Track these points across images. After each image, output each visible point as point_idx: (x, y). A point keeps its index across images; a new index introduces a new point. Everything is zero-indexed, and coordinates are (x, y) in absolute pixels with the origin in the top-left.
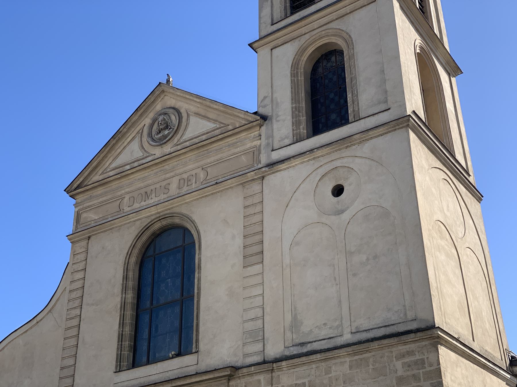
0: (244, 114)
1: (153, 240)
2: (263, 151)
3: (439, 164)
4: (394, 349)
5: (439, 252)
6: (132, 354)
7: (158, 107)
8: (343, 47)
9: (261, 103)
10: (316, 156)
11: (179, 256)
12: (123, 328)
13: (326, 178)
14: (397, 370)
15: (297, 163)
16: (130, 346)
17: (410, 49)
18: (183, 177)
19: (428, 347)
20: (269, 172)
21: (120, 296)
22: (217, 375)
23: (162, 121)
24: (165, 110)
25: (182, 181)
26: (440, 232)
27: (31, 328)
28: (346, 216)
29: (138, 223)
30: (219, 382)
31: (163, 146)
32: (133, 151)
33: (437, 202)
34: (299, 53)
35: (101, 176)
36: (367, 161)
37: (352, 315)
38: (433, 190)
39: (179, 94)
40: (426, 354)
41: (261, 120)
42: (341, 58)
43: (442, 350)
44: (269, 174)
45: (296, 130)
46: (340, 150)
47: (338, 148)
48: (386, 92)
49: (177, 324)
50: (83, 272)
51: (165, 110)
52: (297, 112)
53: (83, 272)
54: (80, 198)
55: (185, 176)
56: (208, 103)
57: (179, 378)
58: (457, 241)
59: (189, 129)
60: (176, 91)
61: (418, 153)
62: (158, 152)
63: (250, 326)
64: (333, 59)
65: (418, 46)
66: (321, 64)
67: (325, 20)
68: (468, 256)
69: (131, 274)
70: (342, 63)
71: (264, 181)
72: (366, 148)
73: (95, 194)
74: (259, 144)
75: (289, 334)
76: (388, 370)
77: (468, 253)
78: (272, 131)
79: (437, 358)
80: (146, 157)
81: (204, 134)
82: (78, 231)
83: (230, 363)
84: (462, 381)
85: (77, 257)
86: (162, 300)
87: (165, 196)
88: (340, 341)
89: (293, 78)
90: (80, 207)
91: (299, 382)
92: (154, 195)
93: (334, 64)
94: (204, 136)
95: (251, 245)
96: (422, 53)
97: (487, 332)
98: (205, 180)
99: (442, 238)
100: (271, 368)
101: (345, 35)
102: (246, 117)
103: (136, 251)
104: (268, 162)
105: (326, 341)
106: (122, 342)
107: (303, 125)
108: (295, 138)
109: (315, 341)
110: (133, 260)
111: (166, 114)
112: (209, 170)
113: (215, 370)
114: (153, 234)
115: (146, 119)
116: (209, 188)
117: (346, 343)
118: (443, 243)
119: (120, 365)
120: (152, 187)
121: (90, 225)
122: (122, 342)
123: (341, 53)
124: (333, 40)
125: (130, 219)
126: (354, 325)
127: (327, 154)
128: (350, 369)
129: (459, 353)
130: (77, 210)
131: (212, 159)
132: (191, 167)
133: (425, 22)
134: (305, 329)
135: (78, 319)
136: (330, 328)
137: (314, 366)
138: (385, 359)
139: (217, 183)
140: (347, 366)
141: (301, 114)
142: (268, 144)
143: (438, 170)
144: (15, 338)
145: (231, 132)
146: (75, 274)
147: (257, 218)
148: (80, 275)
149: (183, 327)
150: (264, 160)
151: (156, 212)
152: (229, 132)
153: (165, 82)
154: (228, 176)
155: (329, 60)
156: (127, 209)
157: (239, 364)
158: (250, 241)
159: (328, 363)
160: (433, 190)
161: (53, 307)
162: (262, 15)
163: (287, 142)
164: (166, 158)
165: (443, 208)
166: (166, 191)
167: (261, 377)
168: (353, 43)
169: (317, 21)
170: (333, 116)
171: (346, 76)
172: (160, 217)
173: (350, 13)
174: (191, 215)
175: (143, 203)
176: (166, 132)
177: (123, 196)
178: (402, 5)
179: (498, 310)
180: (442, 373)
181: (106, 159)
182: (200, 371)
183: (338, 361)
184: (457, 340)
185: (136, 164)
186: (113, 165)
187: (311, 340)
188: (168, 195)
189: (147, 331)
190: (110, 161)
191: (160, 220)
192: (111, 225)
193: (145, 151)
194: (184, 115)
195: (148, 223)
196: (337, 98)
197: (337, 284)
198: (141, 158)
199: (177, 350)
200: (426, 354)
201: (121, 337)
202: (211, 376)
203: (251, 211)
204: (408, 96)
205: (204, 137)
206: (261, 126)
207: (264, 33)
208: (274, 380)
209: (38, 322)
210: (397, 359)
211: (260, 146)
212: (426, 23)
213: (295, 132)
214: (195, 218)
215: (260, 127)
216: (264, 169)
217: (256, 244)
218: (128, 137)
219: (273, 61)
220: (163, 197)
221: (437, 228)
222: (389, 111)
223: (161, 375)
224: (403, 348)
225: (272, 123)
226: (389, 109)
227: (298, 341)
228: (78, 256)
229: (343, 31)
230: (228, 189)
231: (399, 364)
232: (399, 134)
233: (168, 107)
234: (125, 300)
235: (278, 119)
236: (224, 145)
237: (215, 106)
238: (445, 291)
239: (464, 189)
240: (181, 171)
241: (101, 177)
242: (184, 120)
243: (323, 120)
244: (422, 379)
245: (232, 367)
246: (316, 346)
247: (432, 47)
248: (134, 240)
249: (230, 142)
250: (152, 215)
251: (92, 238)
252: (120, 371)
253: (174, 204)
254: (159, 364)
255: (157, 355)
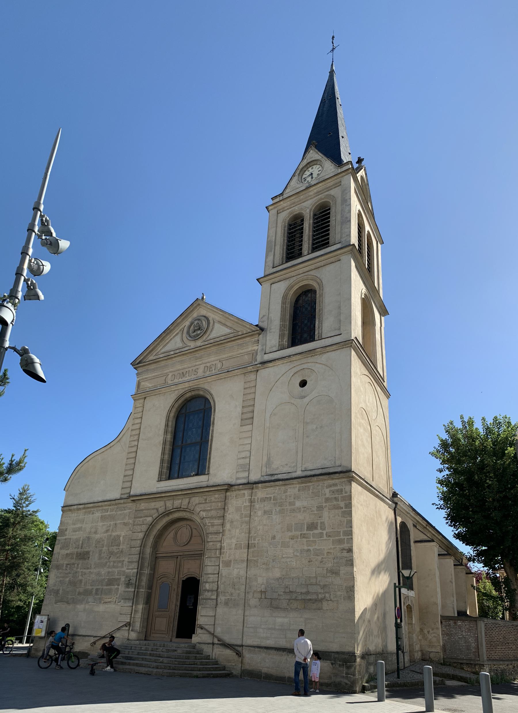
0: (250, 325)
1: (185, 404)
2: (259, 354)
3: (367, 373)
4: (325, 482)
5: (360, 427)
6: (168, 472)
7: (195, 315)
8: (316, 288)
9: (261, 319)
10: (291, 360)
11: (201, 415)
12: (164, 456)
13: (296, 375)
14: (326, 494)
15: (279, 363)
16: (168, 467)
17: (358, 295)
18: (207, 366)
19: (346, 482)
20: (261, 368)
21: (163, 436)
22: (219, 488)
23: (196, 324)
24: (199, 317)
25: (206, 368)
26: (362, 415)
27: (107, 450)
28: (306, 400)
29: (177, 392)
30: (220, 492)
31: (196, 341)
32: (176, 343)
33: (363, 396)
34: (288, 289)
35: (155, 357)
36: (324, 367)
37: (303, 460)
38: (362, 388)
39: (209, 307)
40: (344, 486)
41: (260, 330)
42: (314, 295)
43: (354, 484)
44: (261, 369)
45: (281, 342)
46: (307, 357)
47: (306, 356)
48: (340, 321)
49: (197, 456)
50: (140, 419)
51: (199, 317)
52: (283, 328)
53: (140, 419)
54: (140, 370)
55: (208, 365)
56: (227, 316)
57: (196, 488)
58: (371, 421)
59: (214, 332)
60: (207, 305)
61: (355, 364)
62: (192, 344)
63: (241, 462)
64: (310, 295)
65: (363, 293)
66: (301, 298)
67: (307, 269)
68: (376, 431)
69: (170, 424)
70: (315, 299)
71: (258, 373)
72: (323, 358)
73: (150, 368)
74: (256, 349)
75: (264, 469)
76: (321, 493)
77: (377, 429)
78: (266, 341)
79: (350, 489)
80: (184, 347)
81: (223, 336)
82: (138, 393)
83: (227, 482)
84: (363, 503)
85: (137, 409)
86: (189, 441)
87: (195, 376)
88: (294, 475)
89: (283, 305)
90: (140, 378)
91: (268, 496)
92: (187, 375)
93: (310, 299)
94: (223, 337)
95: (246, 413)
96: (365, 299)
97: (382, 476)
98: (221, 368)
99: (363, 418)
100: (252, 487)
101: (318, 280)
102: (251, 328)
103: (174, 410)
104: (261, 361)
105: (286, 474)
106: (163, 464)
107: (286, 339)
108: (280, 347)
109: (280, 474)
110: (172, 415)
111: (199, 320)
112: (224, 362)
113: (219, 485)
114: (186, 400)
115: (187, 322)
116: (223, 374)
117: (298, 476)
118: (363, 422)
119: (161, 477)
120: (187, 370)
121: (146, 390)
122: (163, 464)
123: (315, 292)
124: (311, 282)
125: (171, 389)
126: (304, 466)
127: (299, 359)
128: (298, 491)
129: (363, 487)
130: (138, 379)
131: (226, 355)
132: (213, 359)
133: (369, 277)
134: (274, 466)
135: (136, 448)
136: (290, 467)
137: (277, 488)
138: (320, 487)
139: (228, 371)
140: (297, 489)
141: (285, 329)
142: (263, 349)
143: (366, 376)
144: (96, 455)
145: (240, 336)
146: (135, 420)
147: (252, 396)
148: (139, 421)
149: (201, 459)
150: (259, 359)
151: (189, 386)
152: (239, 336)
153: (201, 298)
154: (235, 367)
155: (307, 296)
156: (170, 382)
157: (233, 483)
158: (246, 410)
159: (286, 487)
160: (362, 388)
161: (120, 439)
162: (267, 260)
163: (275, 349)
164: (196, 350)
165: (366, 400)
166: (196, 373)
167: (246, 492)
168: (323, 286)
169: (301, 269)
170: (305, 335)
171: (317, 307)
172: (190, 389)
173: (323, 266)
174: (211, 390)
175: (180, 380)
176: (199, 332)
177: (168, 374)
178: (357, 265)
179: (390, 464)
180: (352, 498)
181: (159, 346)
182: (210, 485)
183: (292, 486)
184: (363, 479)
185: (177, 351)
186: (163, 351)
187: (277, 473)
188: (197, 376)
189: (178, 458)
190: (161, 347)
191: (191, 391)
192: (159, 392)
193: (184, 343)
194: (211, 322)
195: (183, 393)
196: (309, 324)
197: (296, 442)
198: (181, 347)
199: (196, 472)
200: (344, 486)
201: (162, 461)
202: (216, 489)
203: (248, 391)
204: (353, 327)
205: (223, 338)
206: (259, 334)
207: (267, 273)
208: (253, 494)
209: (111, 447)
210: (327, 487)
211: (257, 350)
212: (370, 279)
213: (280, 343)
214: (213, 392)
215: (259, 335)
216: (258, 365)
217: (249, 412)
218: (174, 333)
219: (271, 292)
220: (193, 377)
221: (361, 412)
222: (341, 335)
223: (185, 486)
224: (331, 482)
225: (266, 333)
226: (341, 334)
227: (269, 473)
228: (138, 409)
229: (318, 277)
230: (235, 376)
231: (327, 491)
232: (345, 351)
233: (202, 315)
234: (166, 439)
235: (270, 331)
236: (235, 344)
237: (231, 318)
238: (360, 450)
239: (380, 390)
240: (206, 361)
241: (154, 358)
242: (211, 325)
243: (299, 337)
244: (340, 500)
245: (229, 485)
246: (280, 477)
247: (372, 296)
248: (173, 402)
249: (240, 343)
250: (186, 388)
251: (147, 399)
252: (160, 481)
253: (200, 382)
254: (185, 479)
255: (184, 474)
